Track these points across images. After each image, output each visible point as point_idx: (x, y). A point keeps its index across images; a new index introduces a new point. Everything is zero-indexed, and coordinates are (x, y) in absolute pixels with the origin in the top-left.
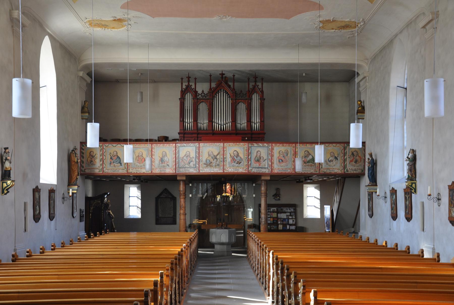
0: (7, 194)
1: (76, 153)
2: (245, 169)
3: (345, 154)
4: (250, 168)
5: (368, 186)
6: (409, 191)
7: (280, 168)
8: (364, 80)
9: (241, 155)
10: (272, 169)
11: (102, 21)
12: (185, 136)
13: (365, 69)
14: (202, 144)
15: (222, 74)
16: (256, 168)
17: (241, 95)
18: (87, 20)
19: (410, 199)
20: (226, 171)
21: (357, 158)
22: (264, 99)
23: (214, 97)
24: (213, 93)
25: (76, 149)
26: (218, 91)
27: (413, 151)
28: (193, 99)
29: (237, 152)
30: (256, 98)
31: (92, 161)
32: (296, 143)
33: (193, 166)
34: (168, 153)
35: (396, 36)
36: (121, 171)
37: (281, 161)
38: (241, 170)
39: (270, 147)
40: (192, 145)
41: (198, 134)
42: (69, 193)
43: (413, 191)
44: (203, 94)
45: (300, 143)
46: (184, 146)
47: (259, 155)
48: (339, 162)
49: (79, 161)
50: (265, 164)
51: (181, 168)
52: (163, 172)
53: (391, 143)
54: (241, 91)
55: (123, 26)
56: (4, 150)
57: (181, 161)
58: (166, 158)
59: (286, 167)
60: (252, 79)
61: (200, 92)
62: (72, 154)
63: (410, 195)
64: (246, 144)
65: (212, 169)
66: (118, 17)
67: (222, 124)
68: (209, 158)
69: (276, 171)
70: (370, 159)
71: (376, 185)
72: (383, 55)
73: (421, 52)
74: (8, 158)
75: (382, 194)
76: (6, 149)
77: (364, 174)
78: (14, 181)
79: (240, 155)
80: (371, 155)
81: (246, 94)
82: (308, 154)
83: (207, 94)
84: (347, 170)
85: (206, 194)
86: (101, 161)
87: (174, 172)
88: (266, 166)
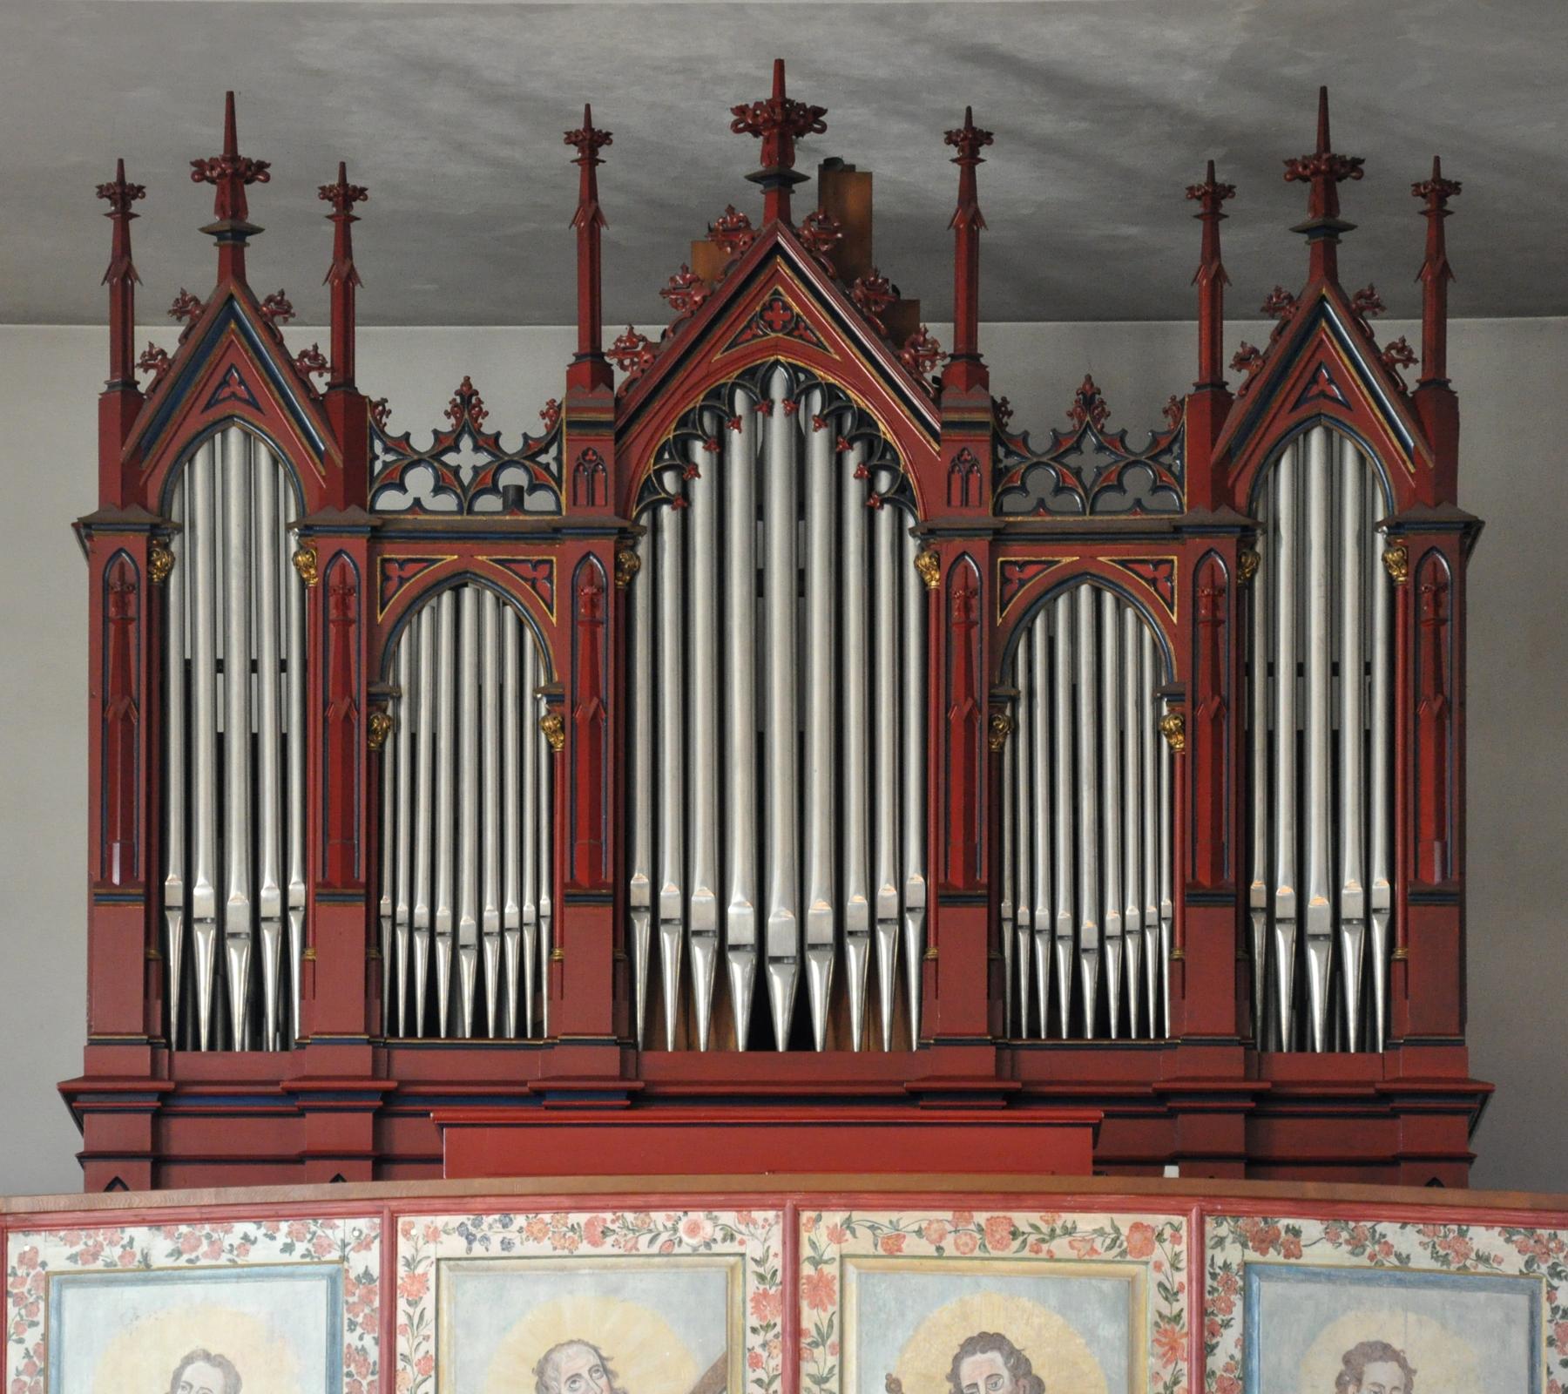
14: (430, 1237)
17: (1090, 460)
22: (1471, 529)
24: (631, 436)
26: (720, 400)
28: (307, 530)
30: (1323, 512)
40: (267, 1243)
41: (390, 1103)
44: (466, 459)
46: (145, 1272)
61: (416, 415)
64: (1171, 1230)
67: (781, 940)
81: (1160, 447)
83: (532, 450)
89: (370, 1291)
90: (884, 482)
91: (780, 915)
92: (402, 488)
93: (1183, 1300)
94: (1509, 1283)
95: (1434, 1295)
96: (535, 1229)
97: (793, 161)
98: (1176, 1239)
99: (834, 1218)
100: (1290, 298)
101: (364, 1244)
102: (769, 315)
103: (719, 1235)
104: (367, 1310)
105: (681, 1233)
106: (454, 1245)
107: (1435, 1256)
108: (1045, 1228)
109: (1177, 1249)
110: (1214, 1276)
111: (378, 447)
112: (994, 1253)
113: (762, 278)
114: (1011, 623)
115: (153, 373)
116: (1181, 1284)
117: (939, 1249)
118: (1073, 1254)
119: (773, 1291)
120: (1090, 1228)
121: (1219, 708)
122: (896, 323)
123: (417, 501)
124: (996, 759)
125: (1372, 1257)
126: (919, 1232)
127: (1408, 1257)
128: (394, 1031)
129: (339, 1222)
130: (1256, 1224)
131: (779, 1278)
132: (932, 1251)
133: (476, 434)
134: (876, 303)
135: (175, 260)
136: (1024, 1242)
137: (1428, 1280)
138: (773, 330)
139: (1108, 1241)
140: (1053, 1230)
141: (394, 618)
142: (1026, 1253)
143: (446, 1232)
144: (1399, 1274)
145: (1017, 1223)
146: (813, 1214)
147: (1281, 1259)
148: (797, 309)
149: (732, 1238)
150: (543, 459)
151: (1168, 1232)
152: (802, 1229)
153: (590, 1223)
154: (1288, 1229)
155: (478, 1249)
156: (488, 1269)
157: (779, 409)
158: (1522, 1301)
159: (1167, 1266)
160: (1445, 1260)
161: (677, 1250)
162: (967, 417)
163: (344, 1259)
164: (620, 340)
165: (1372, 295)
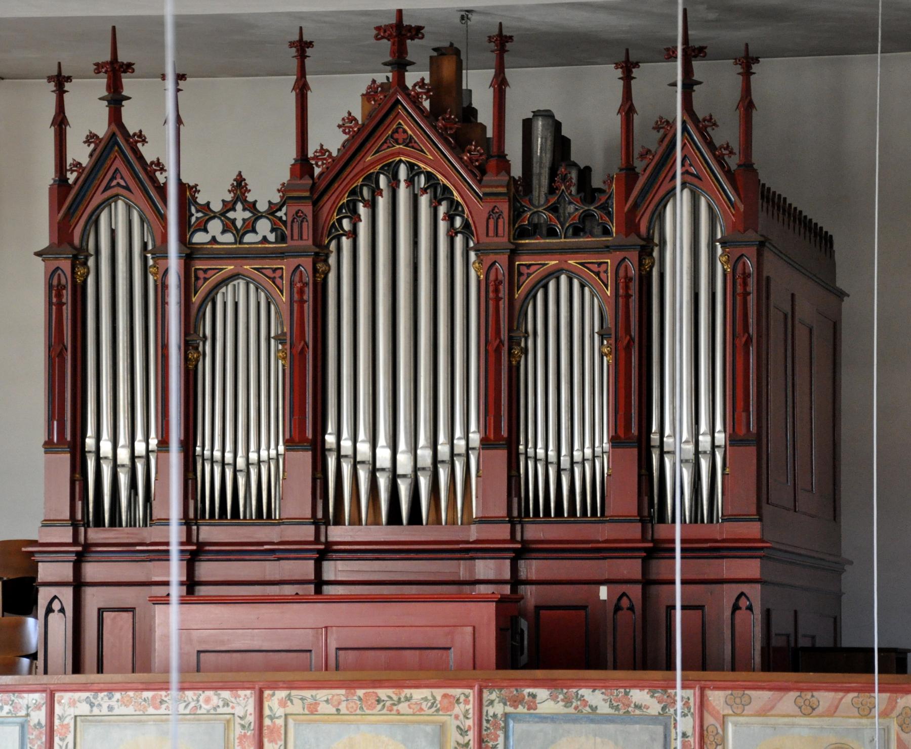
12: (331, 570)
23: (336, 233)
26: (372, 180)
67: (565, 462)
89: (41, 733)
90: (458, 222)
92: (206, 230)
93: (471, 733)
94: (654, 720)
95: (611, 727)
96: (126, 699)
97: (407, 53)
98: (467, 702)
99: (281, 694)
100: (667, 122)
101: (38, 707)
102: (396, 136)
103: (221, 703)
104: (39, 743)
105: (201, 703)
106: (83, 709)
107: (611, 706)
108: (395, 698)
109: (467, 707)
110: (488, 721)
111: (193, 210)
112: (368, 712)
113: (391, 117)
114: (522, 297)
115: (75, 174)
116: (469, 727)
117: (338, 710)
118: (411, 711)
119: (249, 734)
120: (420, 697)
121: (629, 342)
123: (214, 238)
124: (514, 372)
125: (576, 708)
126: (327, 701)
127: (596, 707)
128: (203, 517)
129: (25, 695)
130: (512, 692)
131: (252, 727)
132: (334, 711)
133: (244, 201)
134: (451, 129)
136: (384, 705)
137: (607, 719)
138: (399, 144)
139: (430, 704)
140: (400, 699)
141: (200, 299)
142: (384, 711)
143: (79, 702)
144: (591, 716)
145: (380, 695)
146: (270, 692)
147: (525, 710)
148: (410, 132)
149: (228, 705)
150: (279, 214)
151: (462, 698)
152: (265, 700)
153: (154, 697)
154: (529, 695)
155: (96, 711)
156: (101, 721)
157: (403, 185)
158: (660, 729)
159: (461, 717)
160: (617, 708)
161: (199, 712)
162: (495, 190)
163: (28, 715)
164: (316, 152)
165: (711, 118)
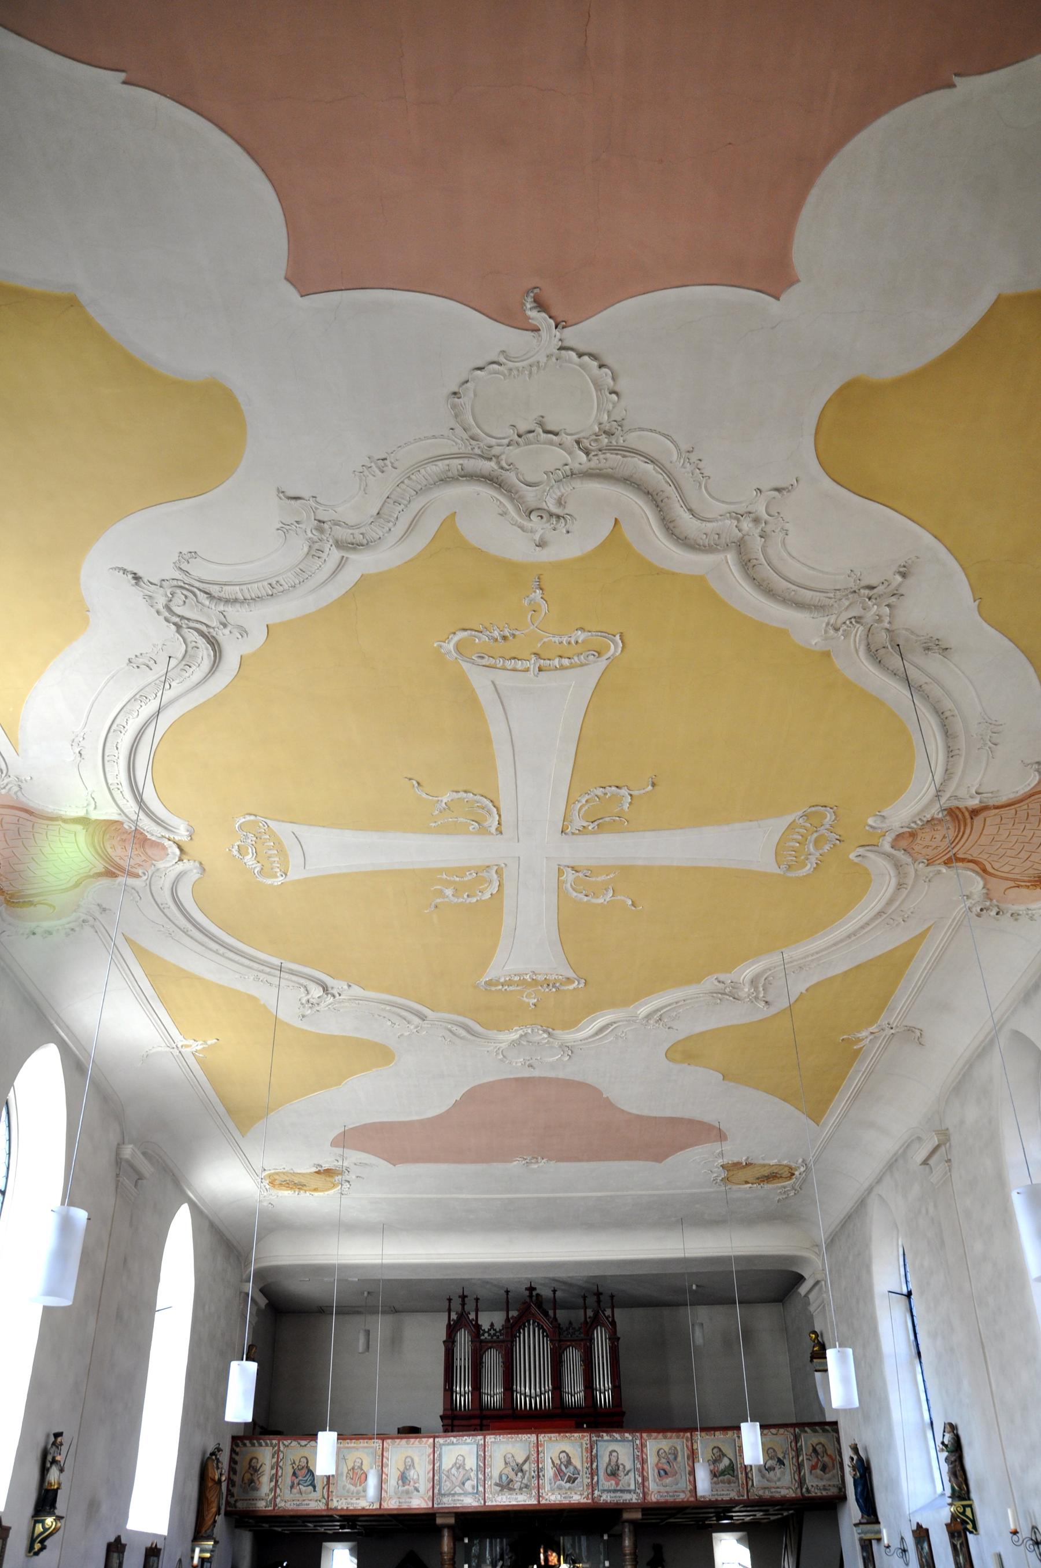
0: (42, 1554)
1: (218, 1460)
2: (586, 1494)
3: (798, 1452)
4: (596, 1493)
5: (860, 1523)
6: (960, 1527)
7: (662, 1489)
8: (817, 1288)
9: (577, 1462)
10: (644, 1493)
11: (295, 1174)
13: (816, 1267)
14: (490, 1439)
15: (531, 1289)
16: (609, 1491)
17: (571, 1331)
18: (267, 1173)
19: (965, 1549)
20: (543, 1502)
21: (826, 1459)
22: (619, 1339)
24: (513, 1328)
25: (219, 1450)
27: (952, 1428)
29: (568, 1455)
30: (600, 1337)
31: (252, 1481)
32: (693, 1430)
33: (470, 1490)
34: (416, 1460)
35: (870, 1190)
36: (312, 1503)
37: (662, 1473)
38: (577, 1497)
39: (638, 1442)
40: (469, 1439)
42: (192, 1558)
43: (970, 1527)
45: (703, 1429)
46: (453, 1444)
47: (614, 1459)
48: (788, 1471)
49: (223, 1478)
50: (630, 1481)
51: (444, 1495)
52: (405, 1506)
53: (896, 1415)
54: (570, 1323)
55: (334, 1186)
56: (52, 1439)
57: (444, 1478)
58: (412, 1472)
59: (674, 1488)
60: (591, 1300)
61: (486, 1326)
62: (210, 1463)
63: (963, 1539)
65: (514, 1496)
66: (326, 1166)
67: (533, 1395)
68: (506, 1471)
69: (653, 1498)
70: (855, 1457)
71: (878, 1522)
72: (849, 1233)
73: (927, 1213)
74: (58, 1458)
75: (896, 1544)
76: (57, 1435)
77: (843, 1498)
78: (62, 1518)
79: (573, 1461)
80: (855, 1449)
81: (580, 1328)
82: (718, 1455)
84: (807, 1489)
85: (500, 1563)
86: (271, 1481)
87: (430, 1505)
88: (632, 1487)
91: (533, 1391)
122: (546, 1314)
135: (456, 1305)
